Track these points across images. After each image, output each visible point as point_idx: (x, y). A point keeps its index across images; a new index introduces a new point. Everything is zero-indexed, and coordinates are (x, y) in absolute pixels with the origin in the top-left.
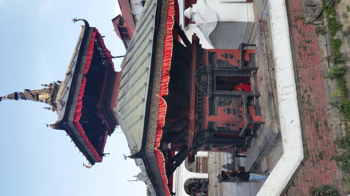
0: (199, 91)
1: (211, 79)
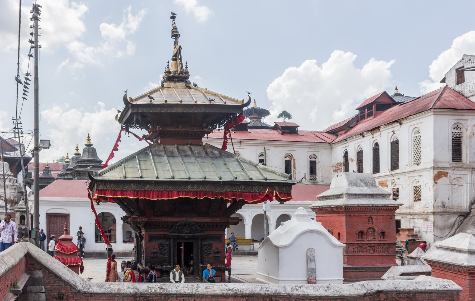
0: (172, 226)
1: (187, 237)
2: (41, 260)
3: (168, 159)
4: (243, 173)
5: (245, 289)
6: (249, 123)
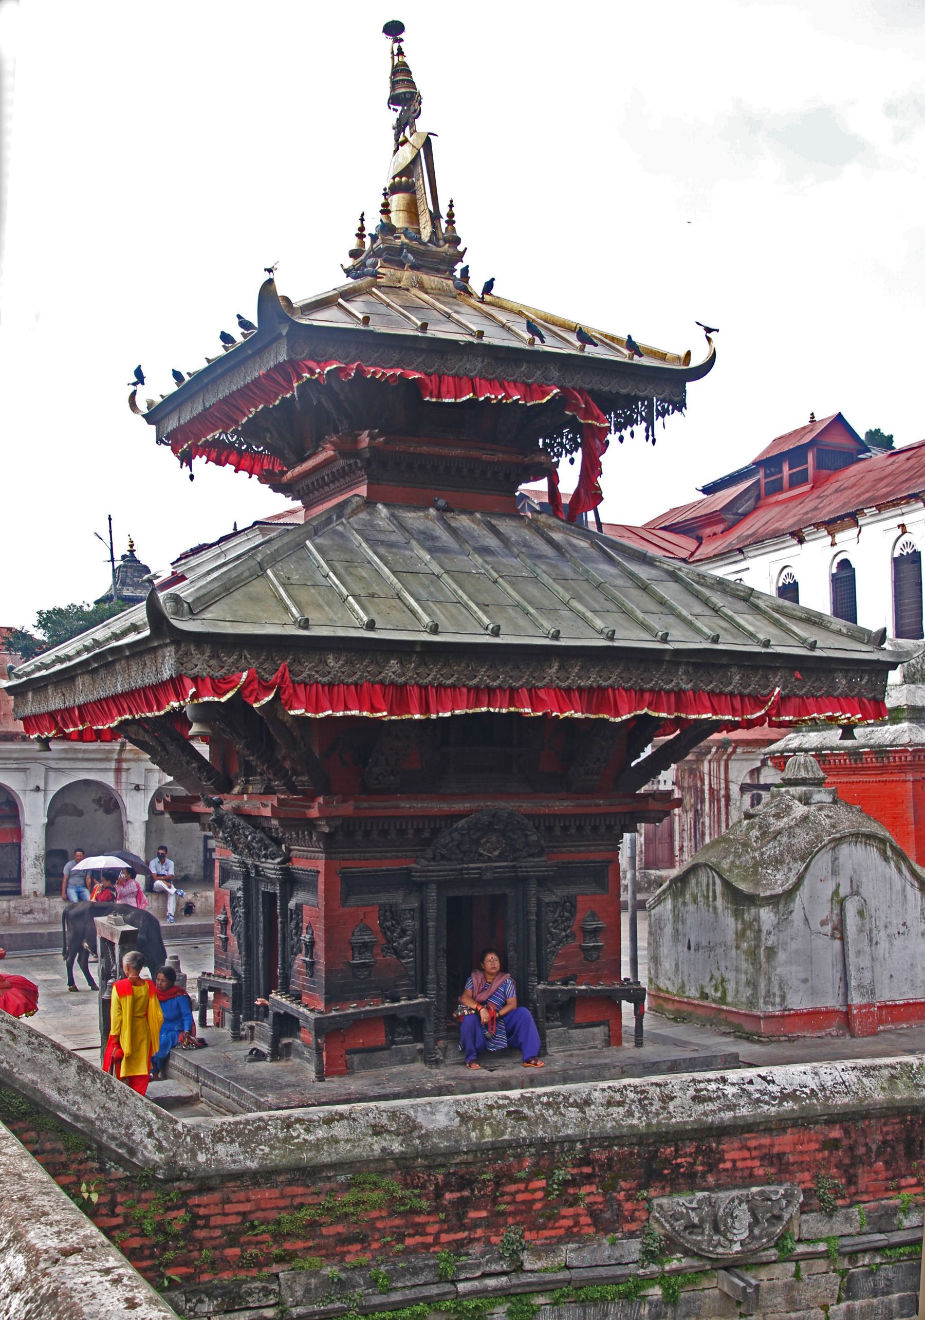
0: (435, 832)
1: (488, 876)
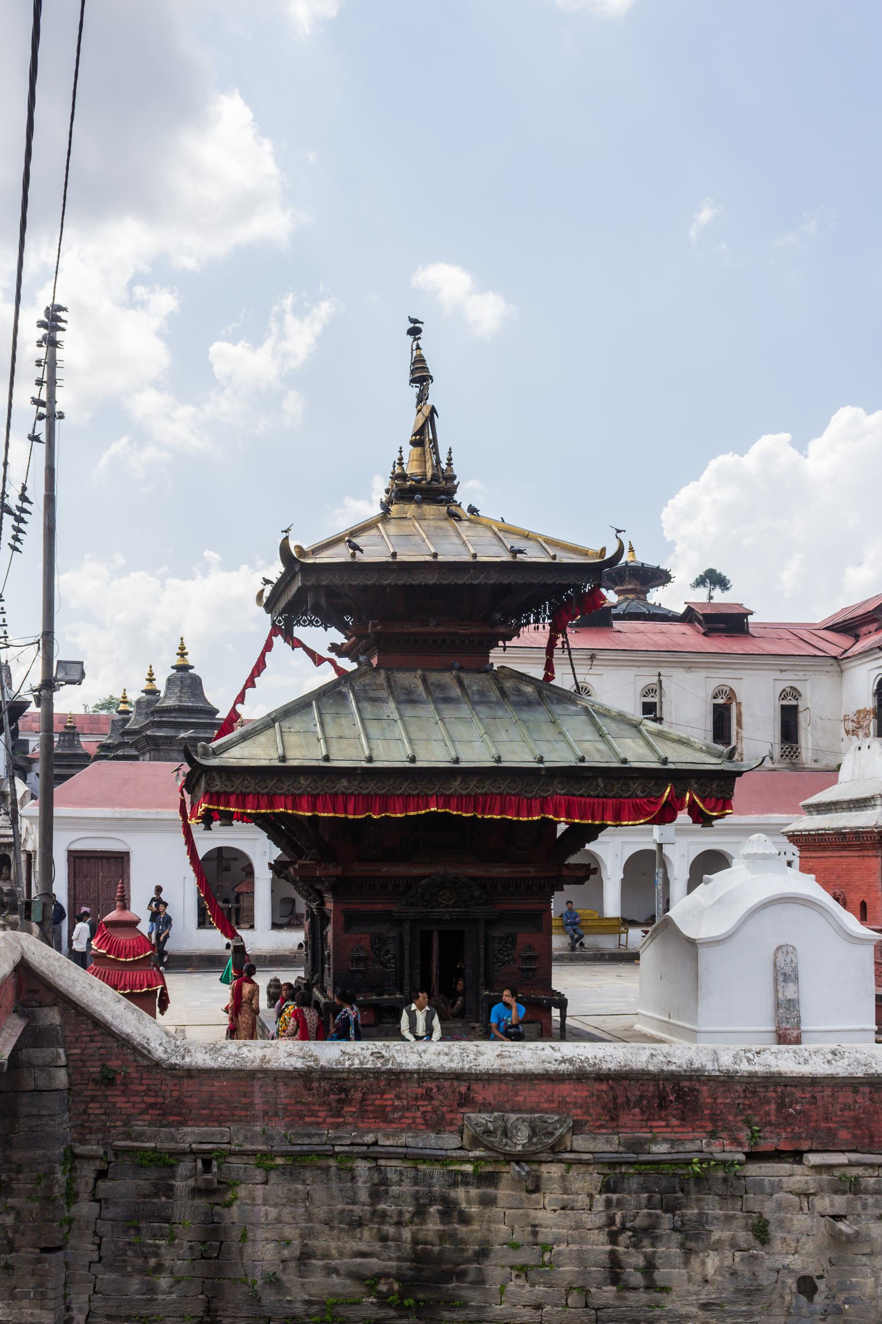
1: (447, 917)
2: (57, 979)
3: (398, 709)
4: (602, 746)
5: (607, 1058)
6: (615, 607)
